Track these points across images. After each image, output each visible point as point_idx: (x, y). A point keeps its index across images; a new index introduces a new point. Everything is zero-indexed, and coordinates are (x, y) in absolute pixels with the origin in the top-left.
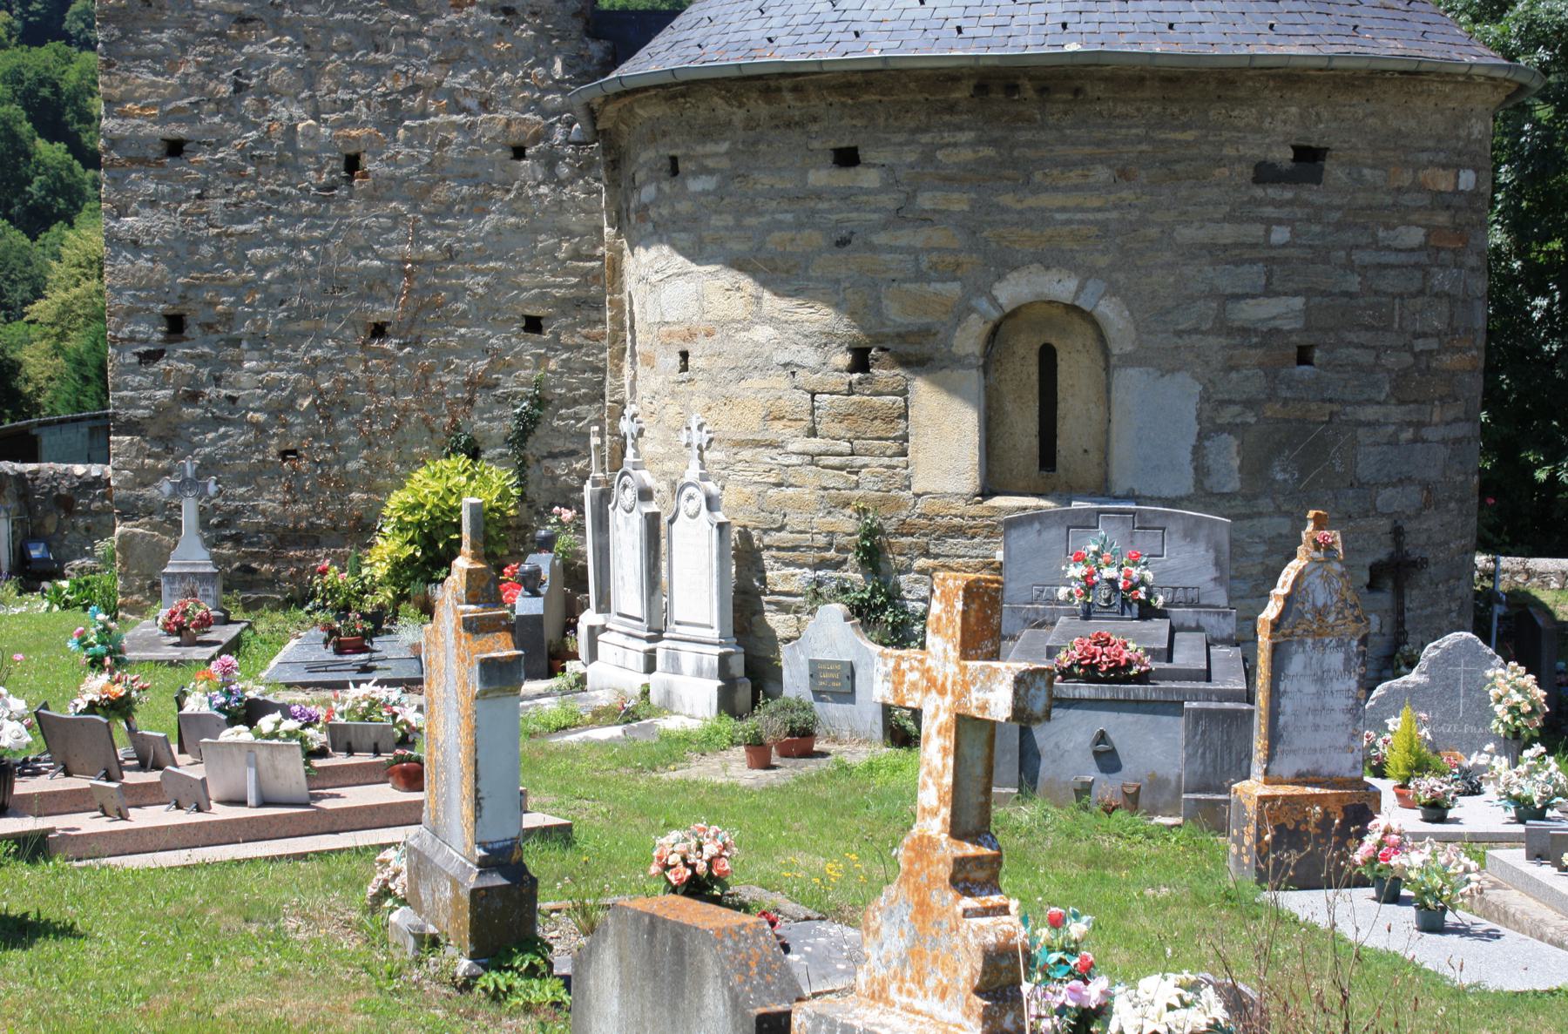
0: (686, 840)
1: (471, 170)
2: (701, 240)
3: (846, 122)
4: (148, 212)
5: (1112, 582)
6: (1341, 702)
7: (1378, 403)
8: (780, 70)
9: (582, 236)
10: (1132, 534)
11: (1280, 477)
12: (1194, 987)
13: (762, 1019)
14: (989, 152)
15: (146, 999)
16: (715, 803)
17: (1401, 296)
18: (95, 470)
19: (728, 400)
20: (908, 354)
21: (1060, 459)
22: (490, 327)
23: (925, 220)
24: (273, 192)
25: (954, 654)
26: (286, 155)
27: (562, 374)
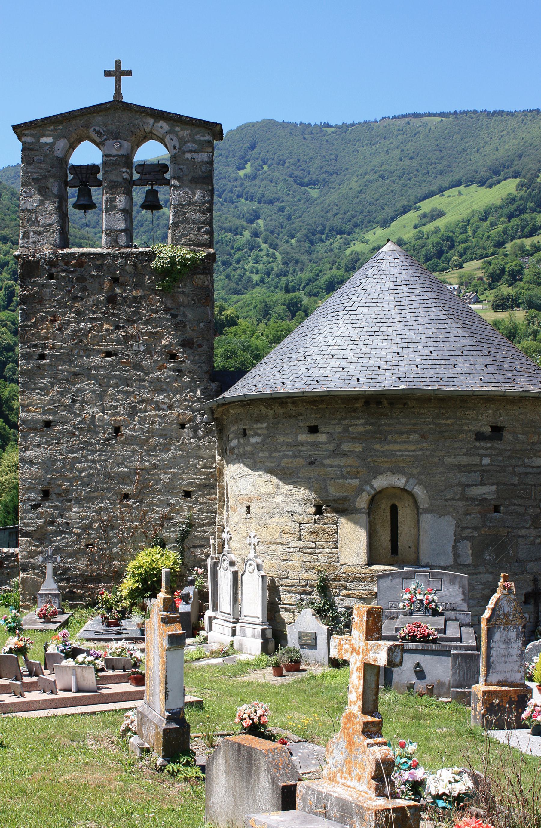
0: (250, 708)
1: (164, 433)
2: (255, 462)
3: (313, 415)
4: (36, 449)
5: (421, 601)
6: (515, 652)
7: (527, 528)
8: (287, 395)
9: (208, 459)
10: (429, 581)
11: (488, 558)
12: (460, 773)
13: (284, 787)
14: (369, 428)
15: (31, 774)
16: (260, 691)
17: (535, 485)
18: (12, 550)
19: (265, 526)
21: (399, 551)
22: (170, 495)
23: (345, 454)
24: (86, 442)
25: (363, 638)
26: (92, 428)
27: (199, 514)
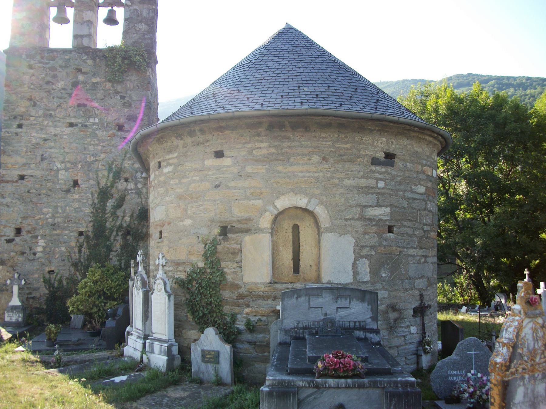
3: (219, 141)
7: (414, 248)
11: (384, 275)
14: (273, 150)
20: (242, 228)
21: (301, 269)
23: (248, 176)
